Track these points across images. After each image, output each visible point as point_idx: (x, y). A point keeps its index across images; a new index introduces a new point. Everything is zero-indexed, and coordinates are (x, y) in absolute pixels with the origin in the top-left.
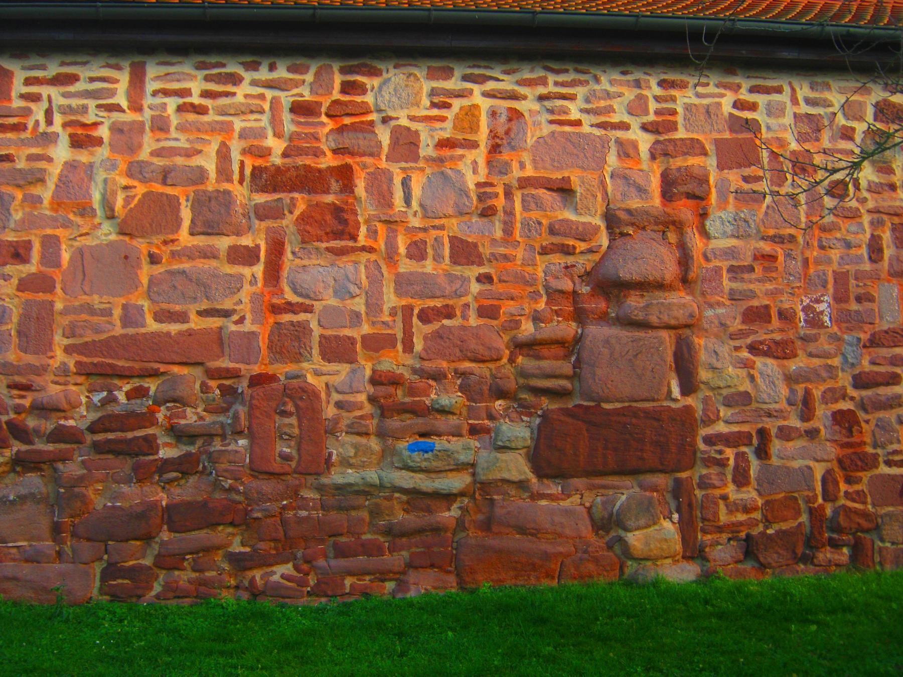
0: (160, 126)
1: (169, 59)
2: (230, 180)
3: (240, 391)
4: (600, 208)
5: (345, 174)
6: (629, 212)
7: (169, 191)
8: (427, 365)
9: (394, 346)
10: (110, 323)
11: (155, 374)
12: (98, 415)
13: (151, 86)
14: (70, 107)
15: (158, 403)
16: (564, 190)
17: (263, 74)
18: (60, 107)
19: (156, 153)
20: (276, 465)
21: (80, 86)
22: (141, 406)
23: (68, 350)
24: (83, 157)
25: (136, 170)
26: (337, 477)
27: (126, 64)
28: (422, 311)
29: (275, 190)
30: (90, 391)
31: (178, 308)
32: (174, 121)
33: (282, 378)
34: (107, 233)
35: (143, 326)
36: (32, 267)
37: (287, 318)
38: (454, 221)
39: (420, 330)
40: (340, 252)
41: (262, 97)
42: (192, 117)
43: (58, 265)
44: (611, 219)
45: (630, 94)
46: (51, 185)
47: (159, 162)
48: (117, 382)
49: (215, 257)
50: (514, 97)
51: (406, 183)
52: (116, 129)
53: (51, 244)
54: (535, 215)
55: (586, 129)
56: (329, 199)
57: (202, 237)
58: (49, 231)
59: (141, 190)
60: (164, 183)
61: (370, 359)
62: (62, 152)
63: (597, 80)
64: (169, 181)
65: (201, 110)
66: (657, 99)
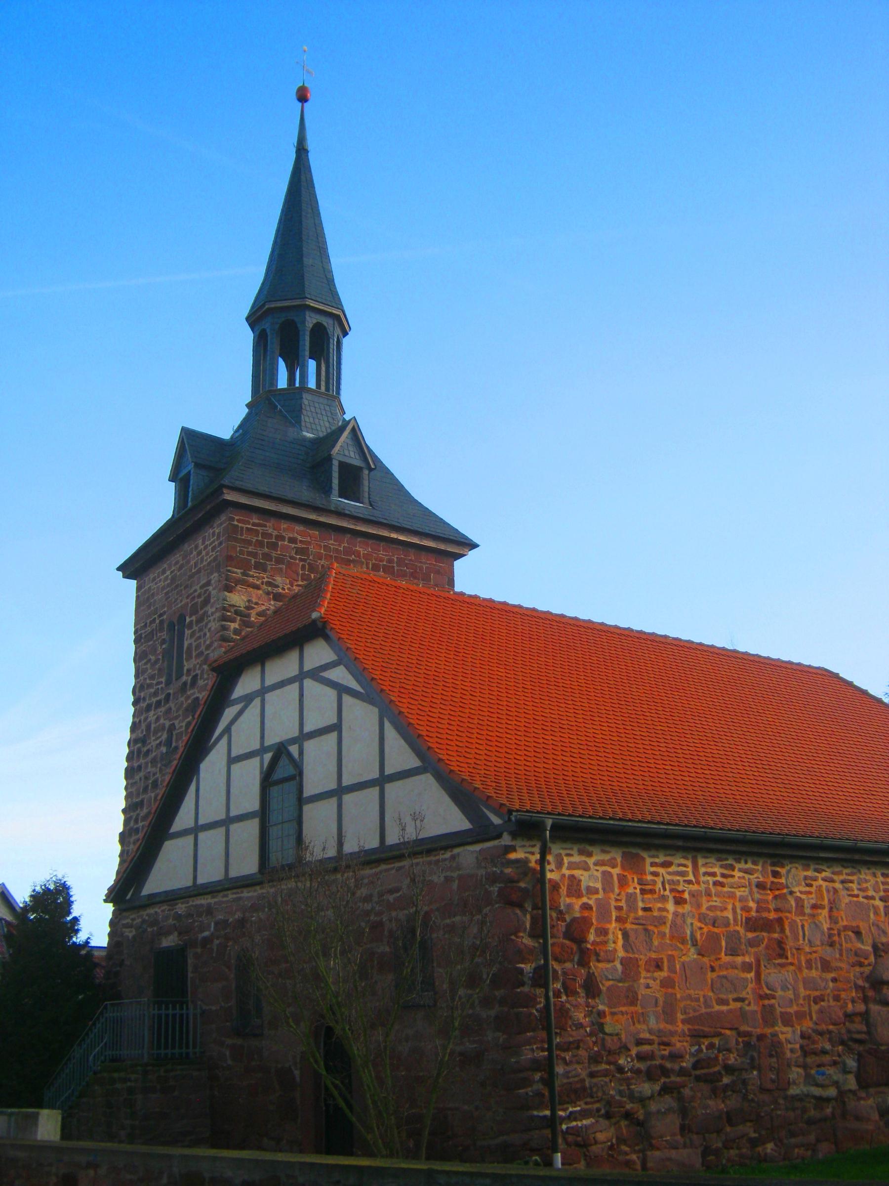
0: (709, 894)
1: (706, 855)
2: (737, 925)
3: (752, 1043)
4: (870, 941)
5: (780, 921)
6: (883, 944)
7: (716, 930)
8: (819, 1028)
9: (806, 1018)
10: (699, 1006)
11: (718, 1034)
12: (695, 1059)
13: (702, 870)
14: (673, 881)
15: (719, 1051)
16: (858, 933)
17: (742, 865)
18: (669, 881)
19: (709, 908)
20: (769, 1085)
21: (673, 869)
22: (712, 1053)
23: (683, 1021)
24: (680, 910)
25: (702, 918)
26: (793, 1091)
27: (690, 856)
28: (814, 998)
29: (755, 931)
30: (691, 1046)
31: (567, 942)
32: (713, 891)
33: (769, 1036)
34: (692, 954)
35: (713, 1008)
36: (664, 974)
37: (766, 1002)
38: (820, 948)
39: (815, 1008)
40: (782, 966)
41: (744, 877)
42: (719, 888)
43: (675, 972)
44: (875, 947)
45: (873, 881)
46: (668, 925)
47: (711, 914)
48: (702, 1040)
49: (737, 968)
50: (832, 881)
51: (803, 926)
52: (692, 895)
53: (671, 958)
54: (849, 945)
55: (861, 899)
56: (776, 935)
57: (730, 957)
58: (670, 953)
59: (705, 930)
60: (714, 926)
61: (799, 1024)
62: (671, 906)
63: (860, 872)
64: (716, 925)
65: (722, 885)
66: (883, 883)
